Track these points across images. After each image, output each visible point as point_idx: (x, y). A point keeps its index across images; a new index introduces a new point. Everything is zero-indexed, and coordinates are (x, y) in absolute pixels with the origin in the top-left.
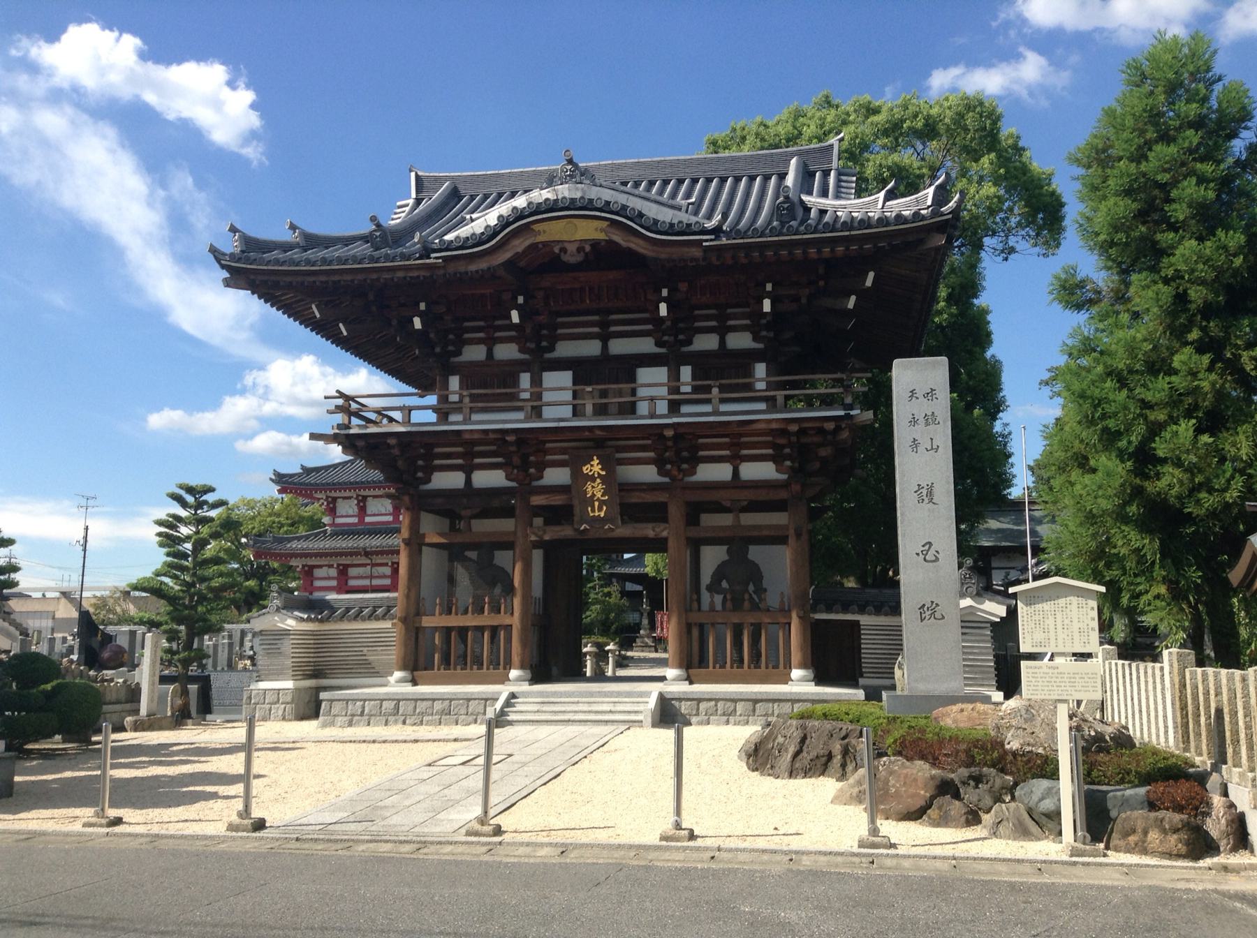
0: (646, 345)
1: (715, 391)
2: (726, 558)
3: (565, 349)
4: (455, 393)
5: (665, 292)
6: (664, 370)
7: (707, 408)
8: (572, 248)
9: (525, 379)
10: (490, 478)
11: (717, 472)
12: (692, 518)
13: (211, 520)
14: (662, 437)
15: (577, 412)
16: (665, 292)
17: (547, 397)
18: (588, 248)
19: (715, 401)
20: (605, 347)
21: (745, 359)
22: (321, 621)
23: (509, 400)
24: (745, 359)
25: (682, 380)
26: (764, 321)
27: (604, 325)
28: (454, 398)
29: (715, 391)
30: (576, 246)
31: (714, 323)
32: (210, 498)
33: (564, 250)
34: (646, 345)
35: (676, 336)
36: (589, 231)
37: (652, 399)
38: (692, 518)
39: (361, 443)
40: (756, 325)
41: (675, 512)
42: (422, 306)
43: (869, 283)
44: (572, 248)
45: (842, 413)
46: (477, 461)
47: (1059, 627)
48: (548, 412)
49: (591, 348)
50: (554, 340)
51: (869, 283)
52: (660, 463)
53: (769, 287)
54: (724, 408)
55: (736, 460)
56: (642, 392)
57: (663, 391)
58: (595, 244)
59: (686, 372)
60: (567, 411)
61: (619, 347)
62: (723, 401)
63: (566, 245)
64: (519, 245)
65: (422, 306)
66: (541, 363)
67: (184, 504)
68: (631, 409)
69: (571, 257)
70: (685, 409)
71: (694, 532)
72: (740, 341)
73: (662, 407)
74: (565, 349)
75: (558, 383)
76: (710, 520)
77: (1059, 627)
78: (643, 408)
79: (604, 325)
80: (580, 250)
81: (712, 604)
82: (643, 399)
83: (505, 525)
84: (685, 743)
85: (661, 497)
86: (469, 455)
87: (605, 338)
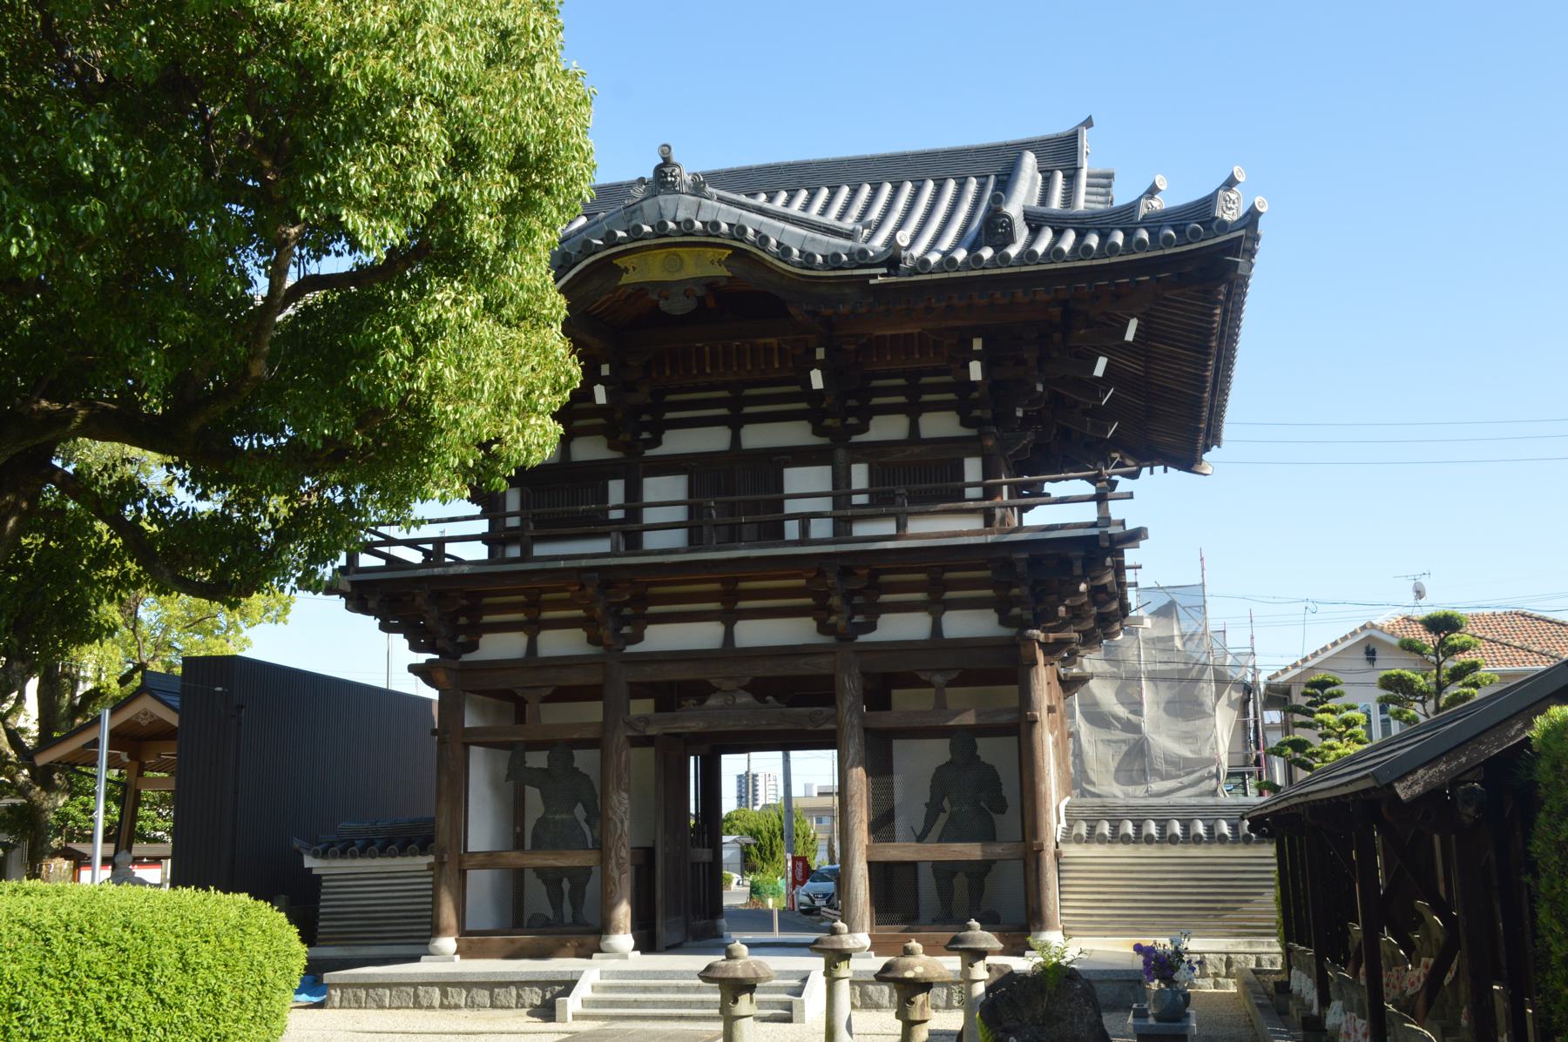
0: (796, 434)
2: (948, 757)
3: (676, 442)
4: (513, 514)
6: (826, 471)
9: (616, 491)
10: (559, 643)
11: (902, 627)
12: (877, 698)
13: (364, 594)
15: (695, 542)
17: (650, 516)
20: (736, 439)
21: (947, 456)
22: (127, 461)
23: (594, 525)
24: (947, 456)
25: (854, 487)
26: (975, 395)
27: (736, 403)
28: (513, 522)
31: (901, 399)
34: (796, 434)
35: (844, 420)
37: (805, 519)
38: (877, 698)
40: (963, 400)
41: (850, 688)
46: (743, 604)
48: (651, 540)
49: (714, 440)
50: (658, 430)
52: (820, 612)
55: (936, 607)
56: (791, 507)
57: (825, 505)
58: (711, 284)
59: (860, 475)
60: (677, 538)
61: (757, 437)
66: (635, 470)
68: (776, 534)
69: (678, 306)
70: (860, 530)
71: (884, 720)
72: (940, 425)
73: (821, 529)
74: (676, 442)
75: (665, 490)
76: (907, 702)
78: (792, 530)
79: (736, 403)
82: (792, 517)
83: (592, 712)
84: (824, 1016)
85: (823, 665)
86: (534, 604)
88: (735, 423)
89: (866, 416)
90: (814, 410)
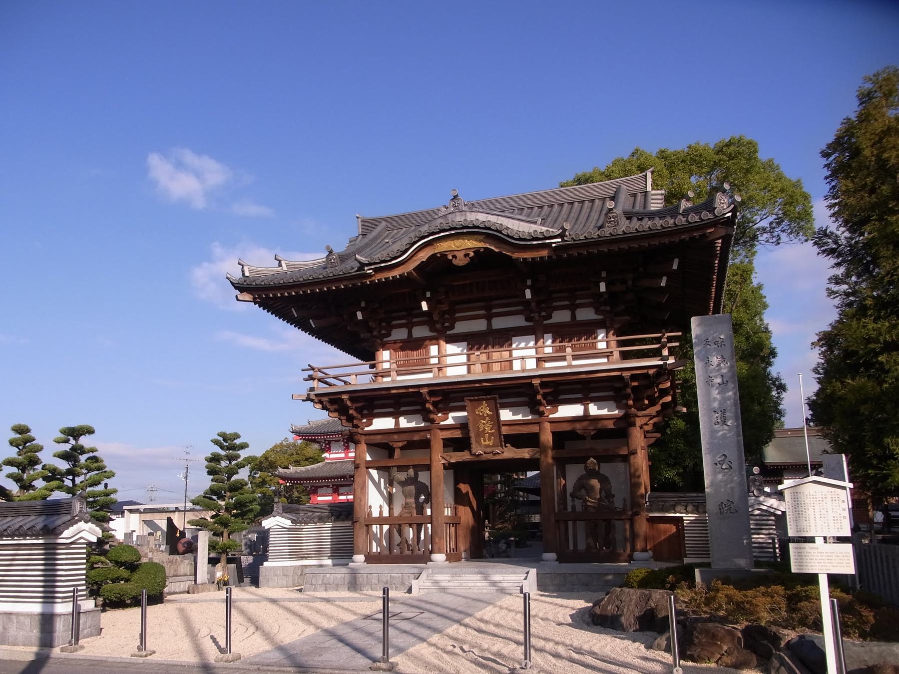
1: (569, 350)
5: (529, 282)
7: (564, 364)
8: (460, 255)
14: (531, 385)
16: (529, 282)
18: (472, 254)
19: (569, 358)
29: (569, 350)
30: (464, 253)
32: (237, 442)
33: (454, 257)
34: (519, 321)
36: (471, 244)
39: (325, 399)
40: (597, 302)
42: (363, 304)
43: (675, 267)
44: (460, 255)
45: (661, 363)
47: (818, 516)
51: (675, 267)
53: (604, 274)
54: (575, 363)
58: (477, 251)
60: (463, 370)
61: (499, 323)
62: (575, 358)
63: (456, 253)
64: (424, 256)
65: (363, 304)
67: (222, 448)
74: (461, 327)
77: (818, 516)
78: (517, 366)
80: (466, 255)
81: (573, 507)
87: (489, 318)
88: (489, 318)
89: (551, 310)
90: (526, 309)
